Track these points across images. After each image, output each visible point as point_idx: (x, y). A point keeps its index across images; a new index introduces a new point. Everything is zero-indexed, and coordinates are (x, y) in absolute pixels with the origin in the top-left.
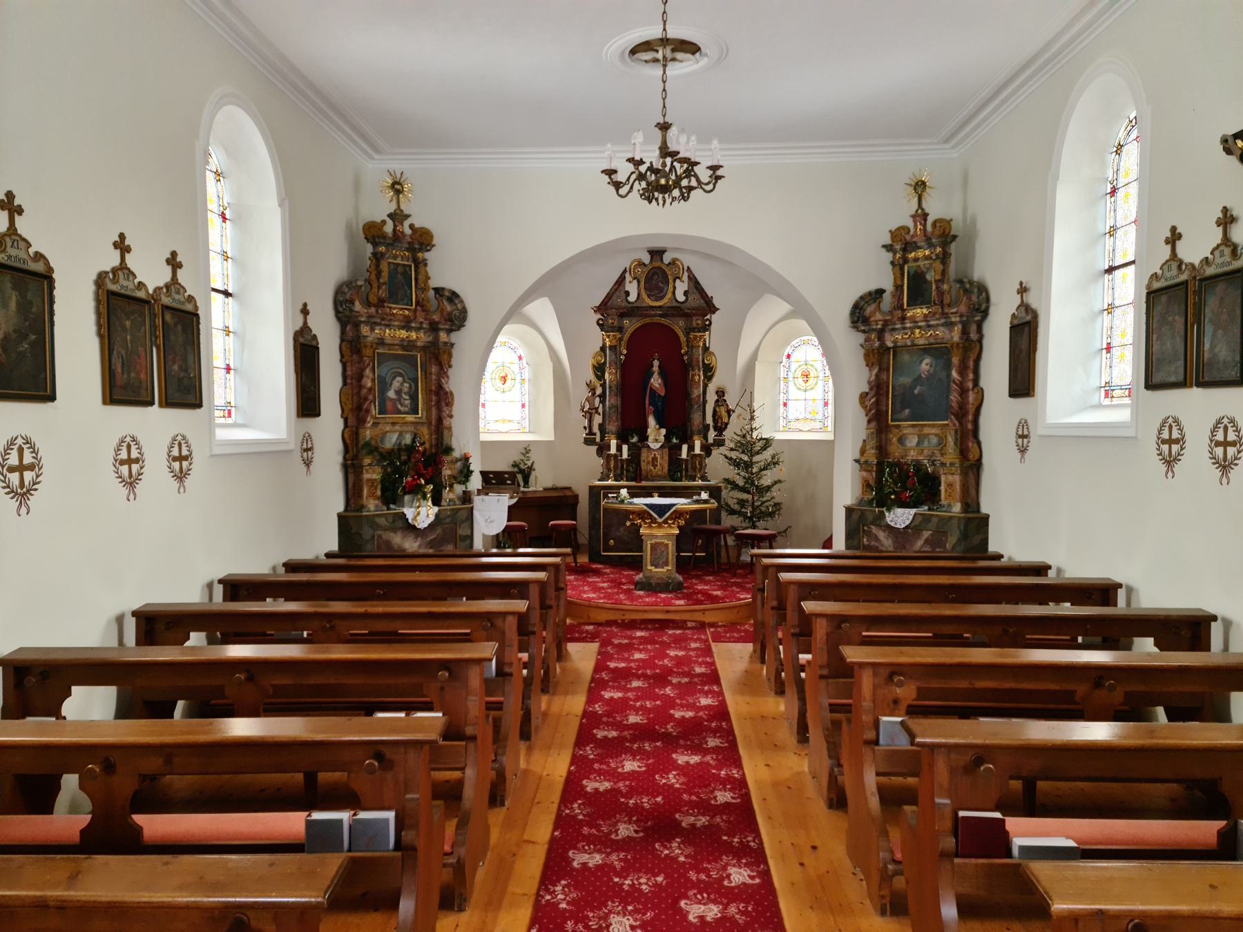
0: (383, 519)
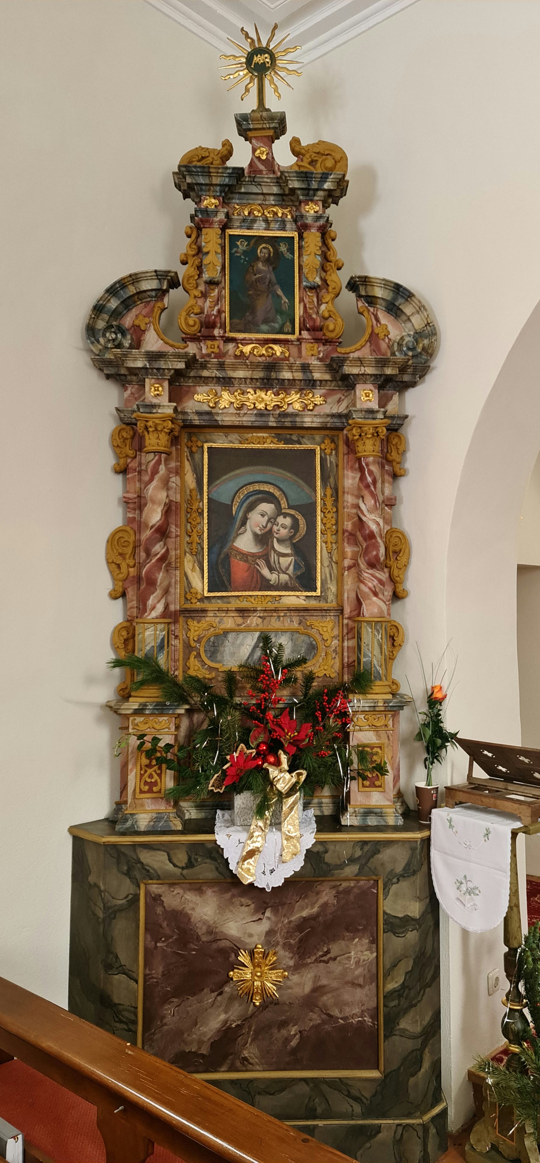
0: (162, 856)
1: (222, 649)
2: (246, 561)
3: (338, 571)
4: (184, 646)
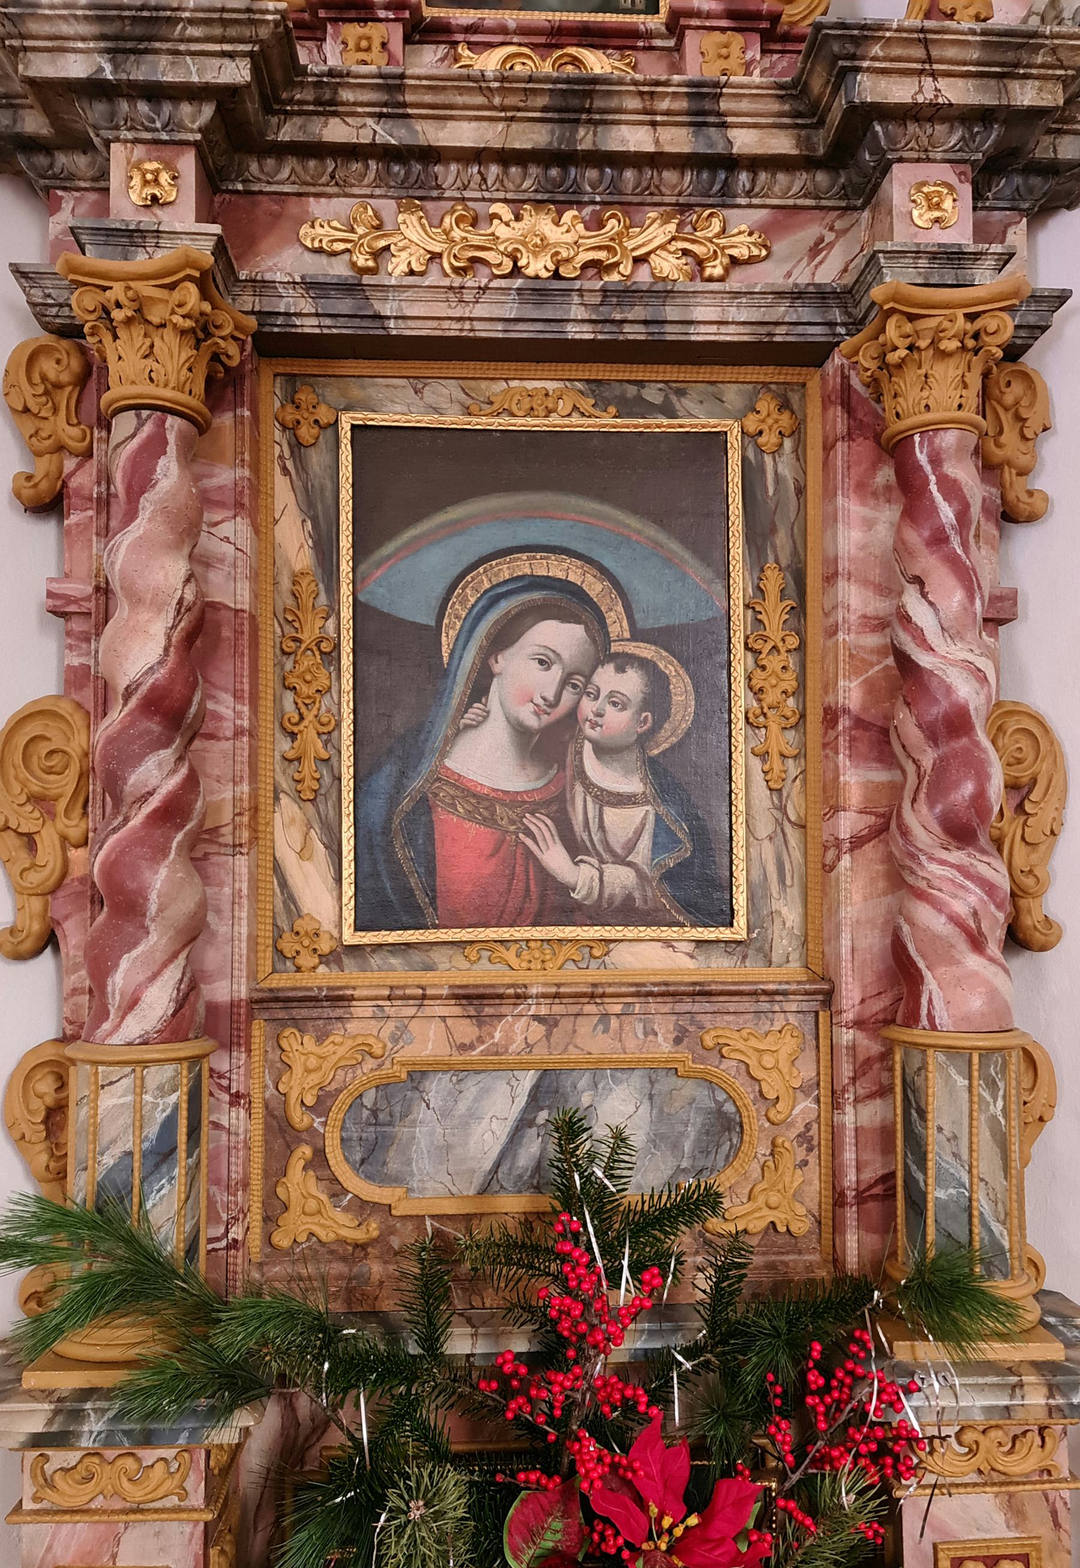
1: (402, 1131)
2: (490, 821)
3: (805, 854)
4: (267, 1127)
